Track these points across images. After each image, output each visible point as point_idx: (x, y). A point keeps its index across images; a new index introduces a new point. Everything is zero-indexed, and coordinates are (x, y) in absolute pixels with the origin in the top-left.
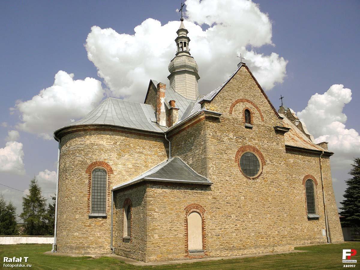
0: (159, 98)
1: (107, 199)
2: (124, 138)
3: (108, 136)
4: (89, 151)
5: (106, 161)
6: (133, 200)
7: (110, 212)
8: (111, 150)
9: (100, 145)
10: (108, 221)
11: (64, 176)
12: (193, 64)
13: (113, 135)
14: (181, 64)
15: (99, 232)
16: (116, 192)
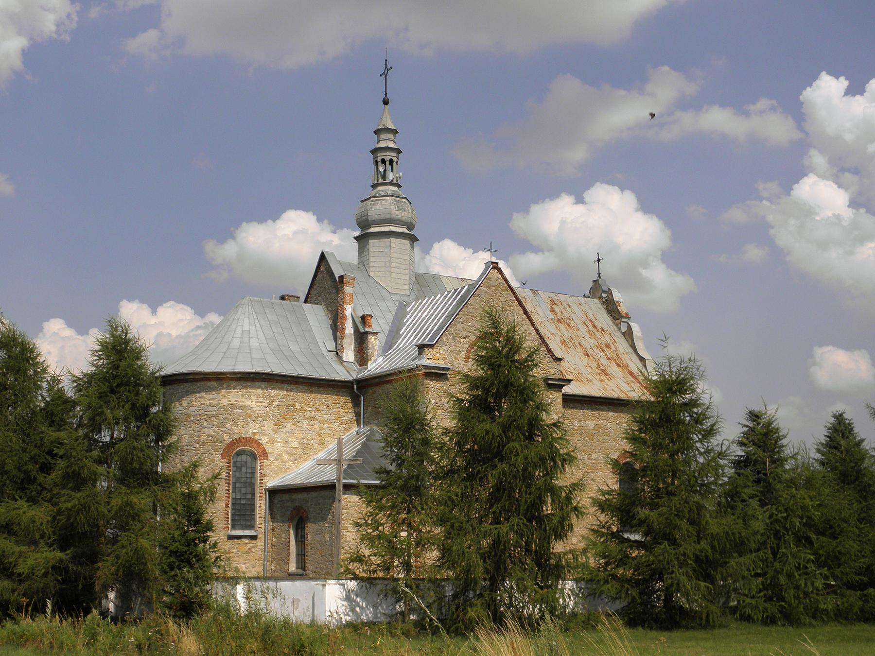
0: (342, 306)
1: (258, 505)
2: (285, 392)
3: (259, 391)
4: (226, 418)
5: (257, 437)
6: (311, 510)
7: (263, 527)
8: (265, 417)
9: (246, 407)
10: (260, 543)
11: (178, 461)
12: (406, 214)
13: (267, 388)
14: (382, 216)
15: (245, 563)
16: (273, 493)
